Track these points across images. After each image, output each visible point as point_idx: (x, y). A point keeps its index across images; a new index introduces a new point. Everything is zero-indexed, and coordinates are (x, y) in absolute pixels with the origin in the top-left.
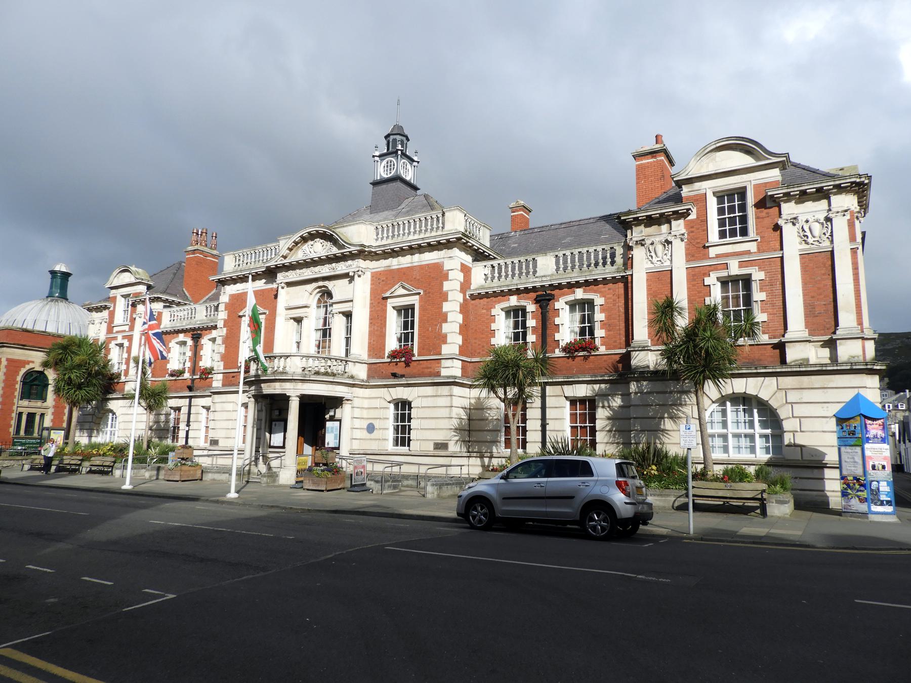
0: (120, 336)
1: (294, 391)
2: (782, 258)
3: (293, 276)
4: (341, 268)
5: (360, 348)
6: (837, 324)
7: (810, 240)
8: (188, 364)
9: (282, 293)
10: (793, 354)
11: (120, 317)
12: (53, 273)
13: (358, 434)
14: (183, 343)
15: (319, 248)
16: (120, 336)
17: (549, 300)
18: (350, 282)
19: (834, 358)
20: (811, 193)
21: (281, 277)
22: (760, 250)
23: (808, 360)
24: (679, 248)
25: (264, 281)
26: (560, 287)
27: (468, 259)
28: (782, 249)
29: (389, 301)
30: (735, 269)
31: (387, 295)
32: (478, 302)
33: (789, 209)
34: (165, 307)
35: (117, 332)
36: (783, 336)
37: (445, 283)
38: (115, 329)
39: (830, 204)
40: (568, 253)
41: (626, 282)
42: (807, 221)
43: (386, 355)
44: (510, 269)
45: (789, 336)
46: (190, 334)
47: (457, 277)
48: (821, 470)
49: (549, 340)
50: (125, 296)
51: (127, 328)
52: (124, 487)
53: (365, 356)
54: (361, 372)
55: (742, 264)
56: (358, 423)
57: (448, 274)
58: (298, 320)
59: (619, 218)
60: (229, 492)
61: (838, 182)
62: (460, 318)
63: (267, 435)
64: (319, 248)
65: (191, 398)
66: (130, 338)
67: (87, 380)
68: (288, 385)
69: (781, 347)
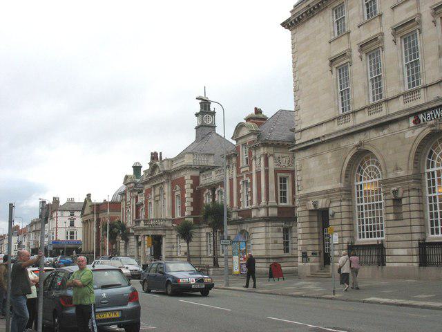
10: (254, 214)
13: (169, 249)
14: (208, 194)
27: (196, 173)
53: (171, 217)
56: (168, 245)
62: (192, 200)
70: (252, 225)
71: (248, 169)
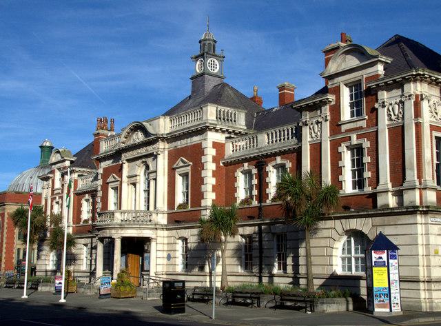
0: (354, 137)
1: (118, 235)
2: (377, 132)
3: (129, 155)
4: (150, 149)
5: (162, 204)
6: (404, 179)
7: (393, 117)
8: (255, 192)
9: (126, 166)
10: (381, 201)
11: (58, 185)
12: (41, 147)
13: (160, 261)
14: (283, 167)
15: (139, 137)
16: (354, 137)
17: (263, 165)
18: (154, 159)
19: (400, 202)
20: (382, 86)
21: (126, 156)
22: (368, 126)
23: (388, 205)
24: (327, 126)
25: (111, 161)
26: (267, 156)
28: (377, 125)
29: (177, 170)
30: (355, 141)
31: (175, 166)
32: (227, 169)
33: (384, 95)
34: (79, 176)
35: (56, 194)
36: (376, 188)
37: (203, 157)
38: (344, 128)
39: (403, 91)
40: (285, 128)
41: (298, 152)
42: (391, 104)
43: (176, 207)
44: (286, 133)
45: (379, 188)
46: (254, 162)
47: (211, 152)
48: (356, 281)
49: (263, 193)
50: (59, 169)
51: (60, 191)
52: (23, 297)
53: (166, 209)
54: (163, 219)
55: (359, 137)
56: (160, 254)
57: (203, 151)
58: (134, 184)
59: (291, 106)
60: (23, 295)
61: (403, 76)
63: (292, 255)
64: (139, 137)
65: (92, 237)
66: (61, 198)
67: (40, 230)
68: (113, 231)
69: (373, 196)
70: (378, 220)
71: (60, 191)
